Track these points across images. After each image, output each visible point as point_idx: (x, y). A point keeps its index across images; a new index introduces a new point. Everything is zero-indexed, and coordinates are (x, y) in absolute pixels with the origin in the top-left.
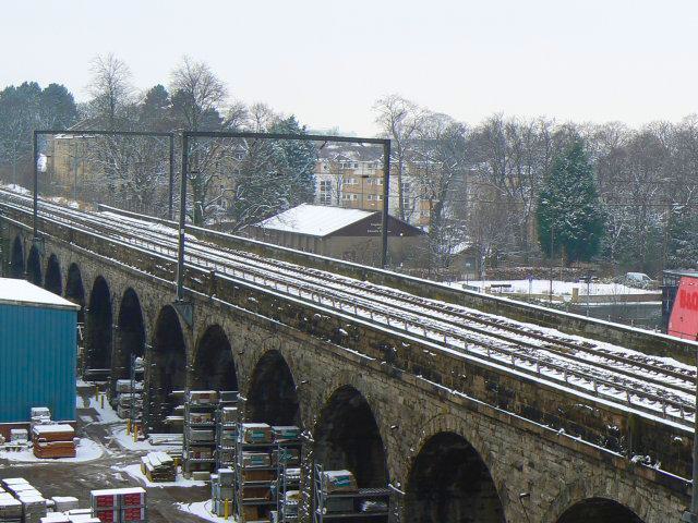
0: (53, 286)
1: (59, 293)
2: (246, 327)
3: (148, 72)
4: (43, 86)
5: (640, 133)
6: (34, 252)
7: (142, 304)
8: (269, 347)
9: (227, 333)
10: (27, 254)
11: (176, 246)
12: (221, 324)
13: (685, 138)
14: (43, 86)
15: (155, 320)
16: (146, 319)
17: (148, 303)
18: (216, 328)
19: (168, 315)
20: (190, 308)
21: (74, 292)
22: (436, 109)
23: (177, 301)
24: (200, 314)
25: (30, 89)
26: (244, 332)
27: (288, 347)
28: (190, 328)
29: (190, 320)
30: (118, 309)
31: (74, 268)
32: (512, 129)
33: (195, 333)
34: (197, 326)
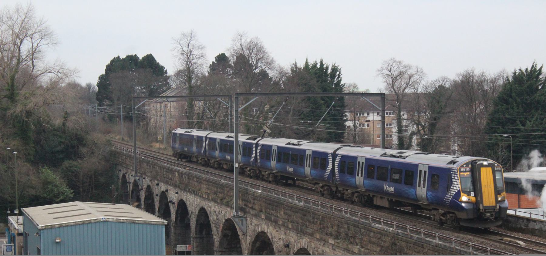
0: (150, 209)
1: (153, 213)
2: (283, 233)
3: (215, 43)
4: (141, 56)
5: (458, 79)
6: (136, 184)
7: (211, 219)
8: (299, 246)
9: (270, 237)
10: (131, 187)
11: (133, 144)
12: (266, 231)
13: (525, 83)
14: (141, 56)
15: (220, 229)
16: (214, 229)
17: (215, 217)
18: (263, 233)
19: (229, 226)
20: (244, 220)
21: (165, 213)
22: (70, 65)
23: (235, 216)
24: (251, 224)
25: (132, 59)
26: (283, 236)
27: (313, 246)
28: (245, 234)
29: (243, 228)
30: (195, 222)
31: (203, 212)
32: (481, 82)
33: (248, 238)
34: (250, 233)
